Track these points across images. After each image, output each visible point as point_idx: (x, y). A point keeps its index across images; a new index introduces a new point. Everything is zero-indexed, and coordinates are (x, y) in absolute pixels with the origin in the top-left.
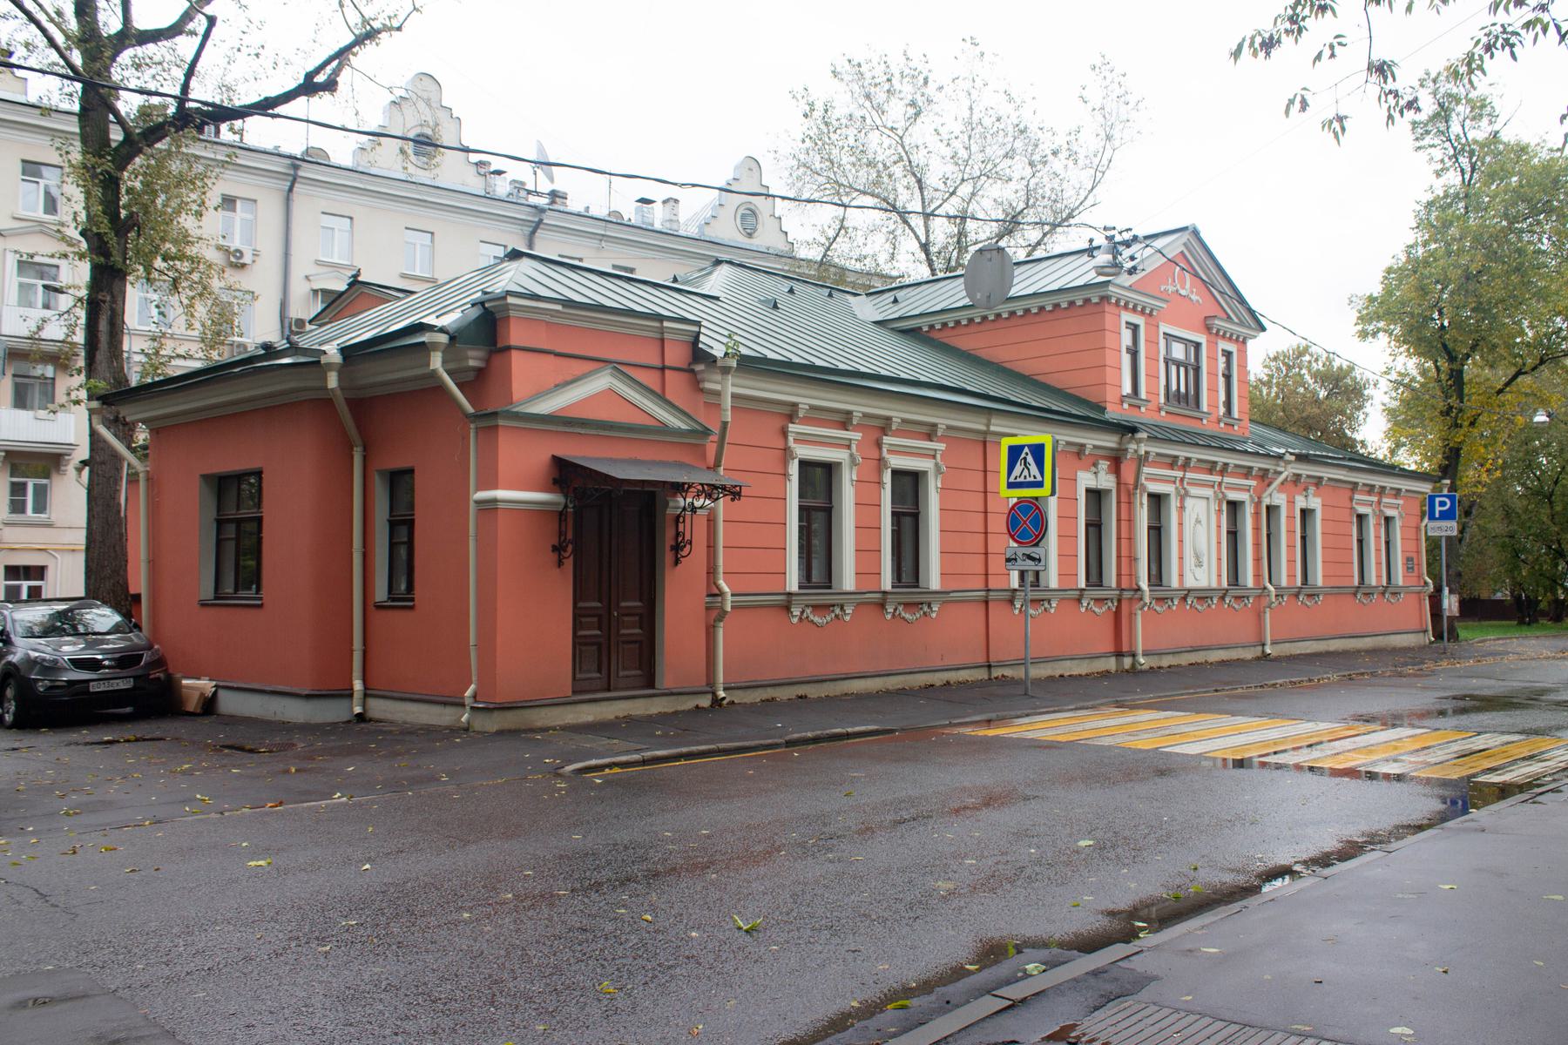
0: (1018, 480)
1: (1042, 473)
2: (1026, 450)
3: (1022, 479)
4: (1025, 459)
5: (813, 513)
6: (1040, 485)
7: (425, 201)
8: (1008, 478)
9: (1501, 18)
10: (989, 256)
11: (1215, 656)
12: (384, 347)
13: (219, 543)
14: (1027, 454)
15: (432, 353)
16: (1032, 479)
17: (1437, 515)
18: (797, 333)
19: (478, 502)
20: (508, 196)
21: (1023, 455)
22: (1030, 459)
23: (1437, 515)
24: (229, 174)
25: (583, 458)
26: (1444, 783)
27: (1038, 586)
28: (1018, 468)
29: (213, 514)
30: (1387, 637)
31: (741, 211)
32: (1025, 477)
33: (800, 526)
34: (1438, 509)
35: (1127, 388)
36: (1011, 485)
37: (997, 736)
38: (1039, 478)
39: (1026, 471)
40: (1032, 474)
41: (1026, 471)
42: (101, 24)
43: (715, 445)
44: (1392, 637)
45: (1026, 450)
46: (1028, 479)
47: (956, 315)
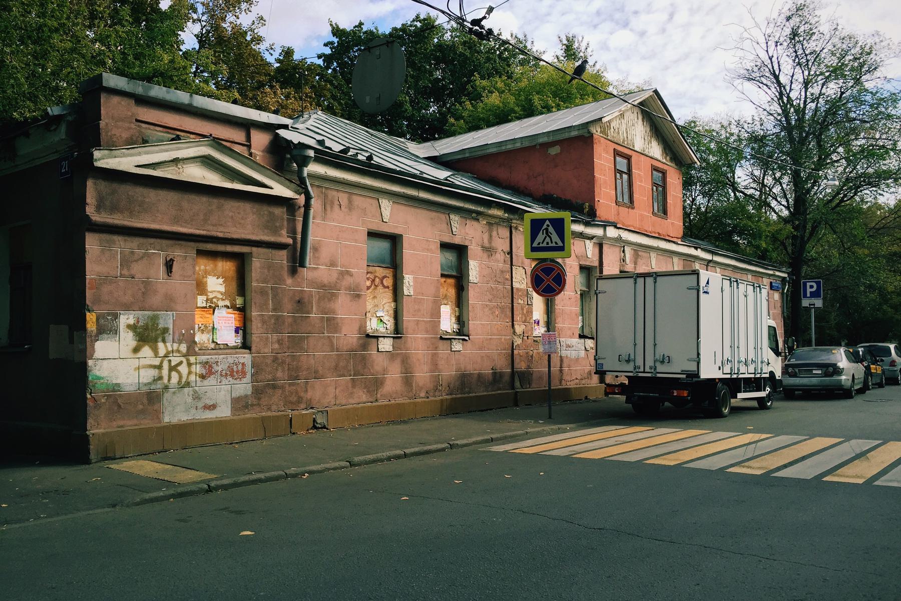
0: (541, 245)
2: (547, 222)
3: (545, 245)
4: (547, 230)
8: (532, 241)
9: (200, 9)
10: (377, 53)
12: (299, 250)
14: (548, 226)
15: (771, 126)
16: (554, 245)
17: (808, 295)
21: (545, 226)
22: (551, 229)
23: (808, 295)
25: (563, 453)
26: (280, 236)
28: (540, 237)
32: (548, 243)
34: (809, 290)
37: (506, 452)
38: (560, 244)
39: (548, 239)
40: (553, 241)
41: (548, 239)
42: (129, 331)
45: (547, 222)
46: (550, 245)
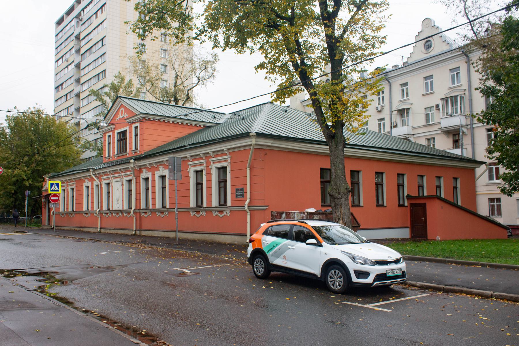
1: (59, 188)
5: (325, 183)
6: (58, 191)
7: (394, 76)
11: (120, 232)
13: (220, 188)
18: (291, 126)
19: (493, 167)
20: (403, 65)
24: (465, 65)
27: (359, 205)
29: (161, 186)
30: (212, 235)
31: (431, 49)
33: (321, 187)
35: (107, 155)
36: (51, 191)
38: (58, 190)
43: (460, 154)
44: (216, 236)
47: (183, 121)
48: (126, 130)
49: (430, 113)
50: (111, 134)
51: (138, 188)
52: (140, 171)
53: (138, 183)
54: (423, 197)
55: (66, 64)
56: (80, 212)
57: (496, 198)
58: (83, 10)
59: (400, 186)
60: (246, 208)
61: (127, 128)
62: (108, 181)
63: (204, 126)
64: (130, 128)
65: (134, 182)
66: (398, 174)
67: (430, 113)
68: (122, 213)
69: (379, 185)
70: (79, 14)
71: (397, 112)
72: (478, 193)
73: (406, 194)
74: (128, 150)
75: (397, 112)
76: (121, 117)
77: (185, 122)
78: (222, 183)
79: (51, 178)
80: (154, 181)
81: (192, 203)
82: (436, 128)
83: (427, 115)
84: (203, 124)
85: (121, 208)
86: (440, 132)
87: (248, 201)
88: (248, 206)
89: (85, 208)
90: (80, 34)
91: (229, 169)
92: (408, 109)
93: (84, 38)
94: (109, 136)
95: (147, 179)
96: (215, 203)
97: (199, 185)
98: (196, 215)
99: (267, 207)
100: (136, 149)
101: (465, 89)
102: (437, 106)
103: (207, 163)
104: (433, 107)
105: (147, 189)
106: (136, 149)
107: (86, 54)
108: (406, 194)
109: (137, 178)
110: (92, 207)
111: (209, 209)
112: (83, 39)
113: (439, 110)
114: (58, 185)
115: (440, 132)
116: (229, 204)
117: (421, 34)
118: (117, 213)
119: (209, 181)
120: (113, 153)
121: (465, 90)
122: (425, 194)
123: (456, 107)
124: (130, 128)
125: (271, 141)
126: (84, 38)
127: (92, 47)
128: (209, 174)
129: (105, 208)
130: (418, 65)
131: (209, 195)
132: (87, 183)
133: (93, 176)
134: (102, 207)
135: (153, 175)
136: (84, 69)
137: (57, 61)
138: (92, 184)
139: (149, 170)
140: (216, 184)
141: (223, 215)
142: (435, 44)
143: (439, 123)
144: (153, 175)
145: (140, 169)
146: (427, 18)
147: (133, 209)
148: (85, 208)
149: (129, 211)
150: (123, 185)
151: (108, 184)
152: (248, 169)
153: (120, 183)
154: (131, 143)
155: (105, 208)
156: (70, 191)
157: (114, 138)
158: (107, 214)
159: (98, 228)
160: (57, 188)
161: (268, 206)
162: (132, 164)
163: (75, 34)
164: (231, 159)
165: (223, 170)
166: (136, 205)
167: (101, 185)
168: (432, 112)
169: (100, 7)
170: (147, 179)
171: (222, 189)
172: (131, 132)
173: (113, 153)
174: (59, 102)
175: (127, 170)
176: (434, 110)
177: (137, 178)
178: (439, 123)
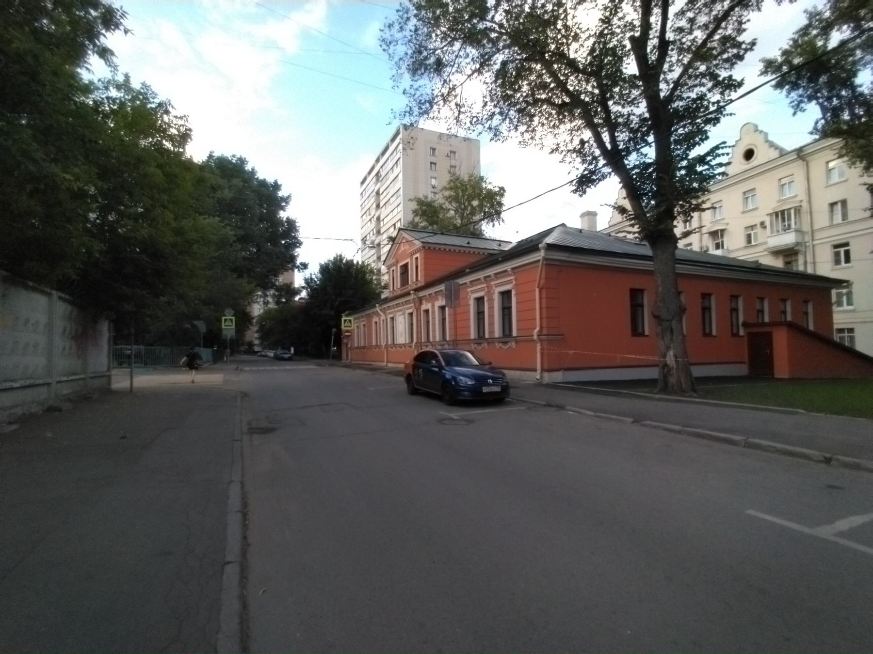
48: (408, 263)
49: (752, 232)
50: (394, 268)
51: (418, 321)
52: (421, 303)
53: (418, 315)
54: (764, 324)
55: (369, 218)
56: (370, 347)
57: (848, 329)
58: (381, 167)
59: (735, 310)
60: (535, 337)
61: (408, 260)
62: (391, 316)
63: (488, 254)
64: (411, 259)
65: (415, 314)
66: (732, 296)
67: (752, 232)
68: (405, 347)
69: (706, 310)
70: (379, 172)
71: (707, 235)
72: (835, 321)
73: (741, 319)
74: (410, 283)
75: (707, 235)
76: (403, 249)
77: (467, 250)
78: (506, 310)
79: (347, 316)
80: (433, 312)
81: (473, 335)
82: (761, 248)
83: (749, 236)
84: (486, 252)
85: (403, 342)
86: (766, 253)
87: (538, 329)
88: (538, 335)
89: (374, 343)
90: (379, 190)
91: (513, 293)
92: (723, 231)
93: (383, 192)
94: (393, 271)
95: (427, 311)
96: (497, 333)
97: (480, 314)
98: (478, 347)
99: (562, 336)
100: (417, 280)
101: (801, 199)
102: (763, 224)
103: (488, 287)
104: (756, 225)
105: (428, 322)
106: (417, 280)
107: (384, 207)
108: (741, 319)
109: (418, 309)
110: (380, 342)
111: (491, 341)
112: (382, 194)
113: (765, 227)
114: (350, 321)
115: (766, 253)
116: (514, 333)
117: (739, 142)
118: (401, 347)
119: (491, 308)
120: (397, 287)
121: (801, 201)
122: (767, 320)
123: (789, 222)
124: (411, 259)
125: (567, 255)
126: (383, 192)
127: (389, 199)
128: (491, 300)
129: (390, 342)
130: (737, 178)
131: (491, 324)
132: (375, 319)
133: (379, 311)
134: (387, 341)
135: (433, 306)
136: (383, 220)
137: (362, 217)
138: (379, 319)
139: (428, 301)
140: (499, 311)
141: (507, 347)
142: (758, 152)
143: (766, 243)
144: (433, 306)
145: (420, 300)
146: (748, 123)
147: (415, 341)
148: (374, 343)
149: (411, 345)
150: (405, 318)
151: (392, 319)
152: (537, 290)
153: (402, 316)
154: (412, 275)
155: (390, 342)
156: (362, 327)
157: (397, 272)
158: (392, 348)
159: (535, 370)
160: (349, 324)
161: (563, 335)
162: (412, 296)
163: (376, 190)
164: (516, 279)
165: (506, 295)
166: (417, 338)
167: (386, 319)
168: (754, 231)
169: (395, 162)
170: (427, 311)
171: (507, 317)
172: (412, 264)
173: (397, 287)
174: (364, 253)
175: (407, 302)
176: (759, 230)
177: (418, 309)
178: (766, 243)
